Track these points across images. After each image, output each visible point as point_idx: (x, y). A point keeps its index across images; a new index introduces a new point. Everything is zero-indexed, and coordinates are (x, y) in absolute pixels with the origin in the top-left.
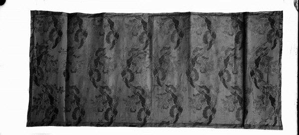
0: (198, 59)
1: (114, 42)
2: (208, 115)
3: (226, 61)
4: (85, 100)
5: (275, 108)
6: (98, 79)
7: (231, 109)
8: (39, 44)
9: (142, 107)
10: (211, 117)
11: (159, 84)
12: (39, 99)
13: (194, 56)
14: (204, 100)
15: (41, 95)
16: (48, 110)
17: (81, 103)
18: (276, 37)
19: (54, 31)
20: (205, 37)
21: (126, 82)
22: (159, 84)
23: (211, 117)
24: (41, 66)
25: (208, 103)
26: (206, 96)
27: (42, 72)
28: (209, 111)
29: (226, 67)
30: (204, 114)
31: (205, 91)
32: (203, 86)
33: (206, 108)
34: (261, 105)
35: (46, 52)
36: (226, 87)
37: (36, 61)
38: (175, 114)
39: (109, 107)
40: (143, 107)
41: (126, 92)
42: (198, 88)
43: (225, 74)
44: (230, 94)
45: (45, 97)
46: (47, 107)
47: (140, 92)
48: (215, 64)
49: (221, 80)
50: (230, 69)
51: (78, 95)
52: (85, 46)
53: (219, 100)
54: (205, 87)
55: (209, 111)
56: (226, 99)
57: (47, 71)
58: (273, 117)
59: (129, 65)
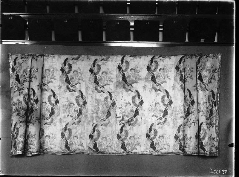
0: (76, 115)
1: (150, 131)
2: (67, 66)
3: (52, 113)
4: (175, 79)
5: (16, 73)
6: (107, 99)
7: (47, 71)
8: (212, 127)
9: (154, 73)
10: (65, 65)
11: (110, 93)
12: (211, 78)
13: (79, 117)
14: (100, 80)
15: (210, 82)
16: (204, 69)
17: (179, 77)
18: (150, 133)
19: (203, 138)
20: (70, 134)
21: (139, 96)
22: (110, 93)
23: (65, 65)
24: (210, 108)
25: (67, 77)
26: (69, 83)
27: (209, 102)
28: (67, 70)
29: (165, 109)
30: (100, 68)
31: (70, 87)
32: (72, 91)
33: (69, 72)
34: (26, 75)
35: (207, 119)
36: (166, 91)
37: (213, 113)
38: (96, 67)
39: (68, 75)
40: (68, 75)
41: (138, 86)
42: (161, 90)
43: (53, 102)
44: (50, 84)
45: (206, 81)
46: (204, 71)
47: (126, 86)
48: (61, 111)
49: (171, 97)
50: (48, 106)
51: (96, 85)
52: (176, 127)
53: (172, 79)
54: (70, 91)
55: (67, 69)
56: (80, 81)
57: (206, 103)
58: (17, 65)
59: (80, 111)
